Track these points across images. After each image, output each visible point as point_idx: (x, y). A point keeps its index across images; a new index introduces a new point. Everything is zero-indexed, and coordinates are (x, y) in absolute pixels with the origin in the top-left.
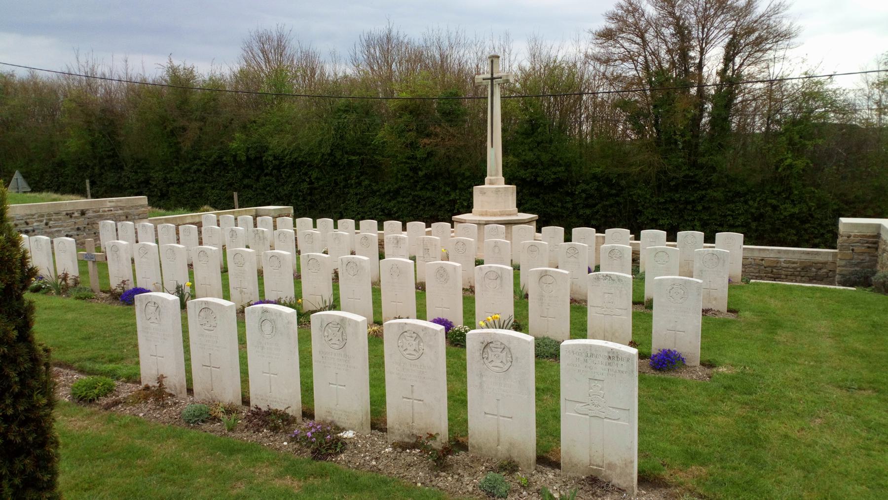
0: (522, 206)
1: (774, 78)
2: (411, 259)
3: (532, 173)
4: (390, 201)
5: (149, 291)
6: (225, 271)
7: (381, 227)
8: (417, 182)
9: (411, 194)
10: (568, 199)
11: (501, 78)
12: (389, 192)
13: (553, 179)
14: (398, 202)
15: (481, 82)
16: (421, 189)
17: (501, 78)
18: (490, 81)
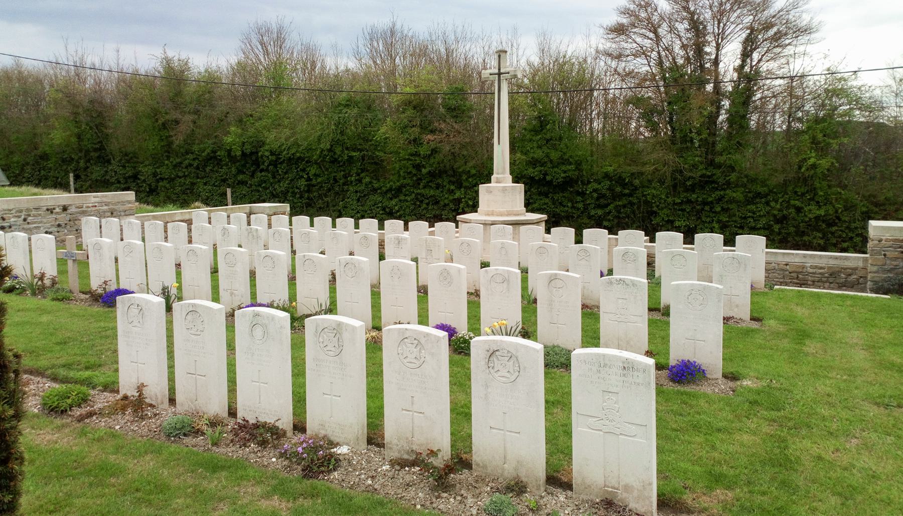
0: (530, 206)
1: (795, 74)
2: (412, 260)
3: (541, 171)
4: (391, 199)
5: (132, 292)
6: (215, 271)
7: (381, 227)
8: (420, 179)
9: (413, 192)
10: (579, 198)
11: (508, 73)
12: (390, 190)
13: (563, 178)
14: (400, 201)
15: (488, 77)
16: (424, 187)
17: (508, 73)
18: (497, 76)
